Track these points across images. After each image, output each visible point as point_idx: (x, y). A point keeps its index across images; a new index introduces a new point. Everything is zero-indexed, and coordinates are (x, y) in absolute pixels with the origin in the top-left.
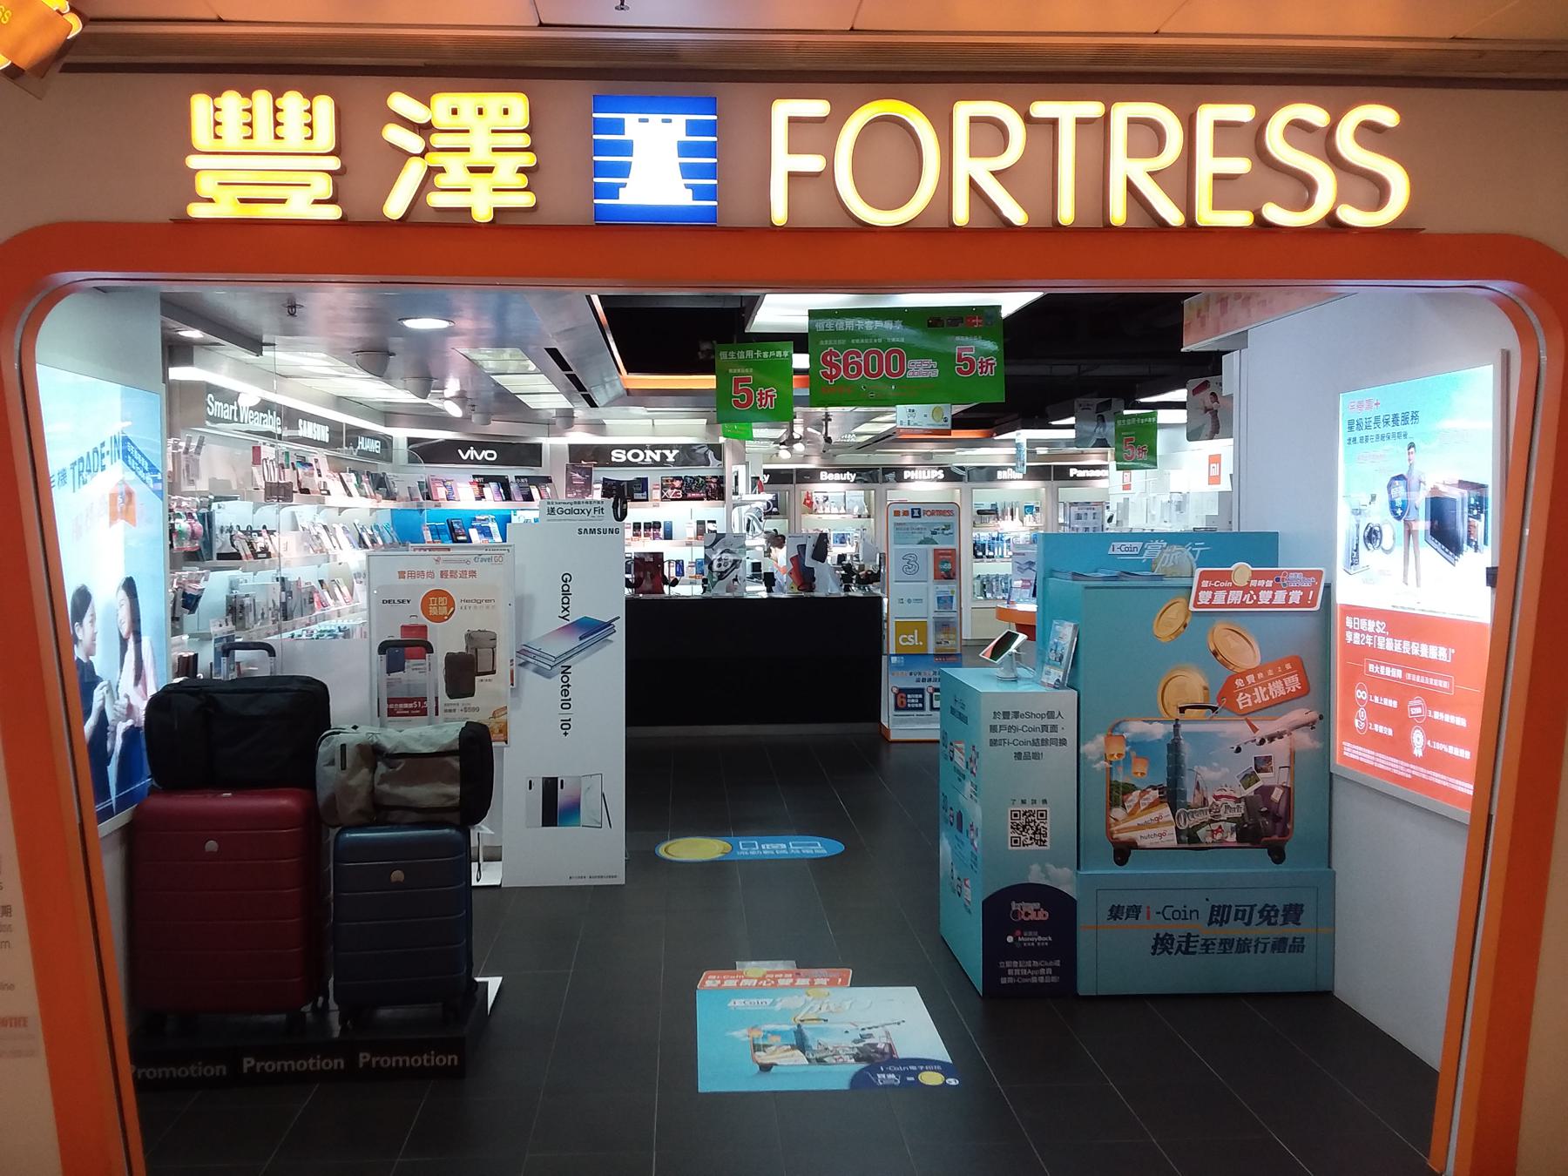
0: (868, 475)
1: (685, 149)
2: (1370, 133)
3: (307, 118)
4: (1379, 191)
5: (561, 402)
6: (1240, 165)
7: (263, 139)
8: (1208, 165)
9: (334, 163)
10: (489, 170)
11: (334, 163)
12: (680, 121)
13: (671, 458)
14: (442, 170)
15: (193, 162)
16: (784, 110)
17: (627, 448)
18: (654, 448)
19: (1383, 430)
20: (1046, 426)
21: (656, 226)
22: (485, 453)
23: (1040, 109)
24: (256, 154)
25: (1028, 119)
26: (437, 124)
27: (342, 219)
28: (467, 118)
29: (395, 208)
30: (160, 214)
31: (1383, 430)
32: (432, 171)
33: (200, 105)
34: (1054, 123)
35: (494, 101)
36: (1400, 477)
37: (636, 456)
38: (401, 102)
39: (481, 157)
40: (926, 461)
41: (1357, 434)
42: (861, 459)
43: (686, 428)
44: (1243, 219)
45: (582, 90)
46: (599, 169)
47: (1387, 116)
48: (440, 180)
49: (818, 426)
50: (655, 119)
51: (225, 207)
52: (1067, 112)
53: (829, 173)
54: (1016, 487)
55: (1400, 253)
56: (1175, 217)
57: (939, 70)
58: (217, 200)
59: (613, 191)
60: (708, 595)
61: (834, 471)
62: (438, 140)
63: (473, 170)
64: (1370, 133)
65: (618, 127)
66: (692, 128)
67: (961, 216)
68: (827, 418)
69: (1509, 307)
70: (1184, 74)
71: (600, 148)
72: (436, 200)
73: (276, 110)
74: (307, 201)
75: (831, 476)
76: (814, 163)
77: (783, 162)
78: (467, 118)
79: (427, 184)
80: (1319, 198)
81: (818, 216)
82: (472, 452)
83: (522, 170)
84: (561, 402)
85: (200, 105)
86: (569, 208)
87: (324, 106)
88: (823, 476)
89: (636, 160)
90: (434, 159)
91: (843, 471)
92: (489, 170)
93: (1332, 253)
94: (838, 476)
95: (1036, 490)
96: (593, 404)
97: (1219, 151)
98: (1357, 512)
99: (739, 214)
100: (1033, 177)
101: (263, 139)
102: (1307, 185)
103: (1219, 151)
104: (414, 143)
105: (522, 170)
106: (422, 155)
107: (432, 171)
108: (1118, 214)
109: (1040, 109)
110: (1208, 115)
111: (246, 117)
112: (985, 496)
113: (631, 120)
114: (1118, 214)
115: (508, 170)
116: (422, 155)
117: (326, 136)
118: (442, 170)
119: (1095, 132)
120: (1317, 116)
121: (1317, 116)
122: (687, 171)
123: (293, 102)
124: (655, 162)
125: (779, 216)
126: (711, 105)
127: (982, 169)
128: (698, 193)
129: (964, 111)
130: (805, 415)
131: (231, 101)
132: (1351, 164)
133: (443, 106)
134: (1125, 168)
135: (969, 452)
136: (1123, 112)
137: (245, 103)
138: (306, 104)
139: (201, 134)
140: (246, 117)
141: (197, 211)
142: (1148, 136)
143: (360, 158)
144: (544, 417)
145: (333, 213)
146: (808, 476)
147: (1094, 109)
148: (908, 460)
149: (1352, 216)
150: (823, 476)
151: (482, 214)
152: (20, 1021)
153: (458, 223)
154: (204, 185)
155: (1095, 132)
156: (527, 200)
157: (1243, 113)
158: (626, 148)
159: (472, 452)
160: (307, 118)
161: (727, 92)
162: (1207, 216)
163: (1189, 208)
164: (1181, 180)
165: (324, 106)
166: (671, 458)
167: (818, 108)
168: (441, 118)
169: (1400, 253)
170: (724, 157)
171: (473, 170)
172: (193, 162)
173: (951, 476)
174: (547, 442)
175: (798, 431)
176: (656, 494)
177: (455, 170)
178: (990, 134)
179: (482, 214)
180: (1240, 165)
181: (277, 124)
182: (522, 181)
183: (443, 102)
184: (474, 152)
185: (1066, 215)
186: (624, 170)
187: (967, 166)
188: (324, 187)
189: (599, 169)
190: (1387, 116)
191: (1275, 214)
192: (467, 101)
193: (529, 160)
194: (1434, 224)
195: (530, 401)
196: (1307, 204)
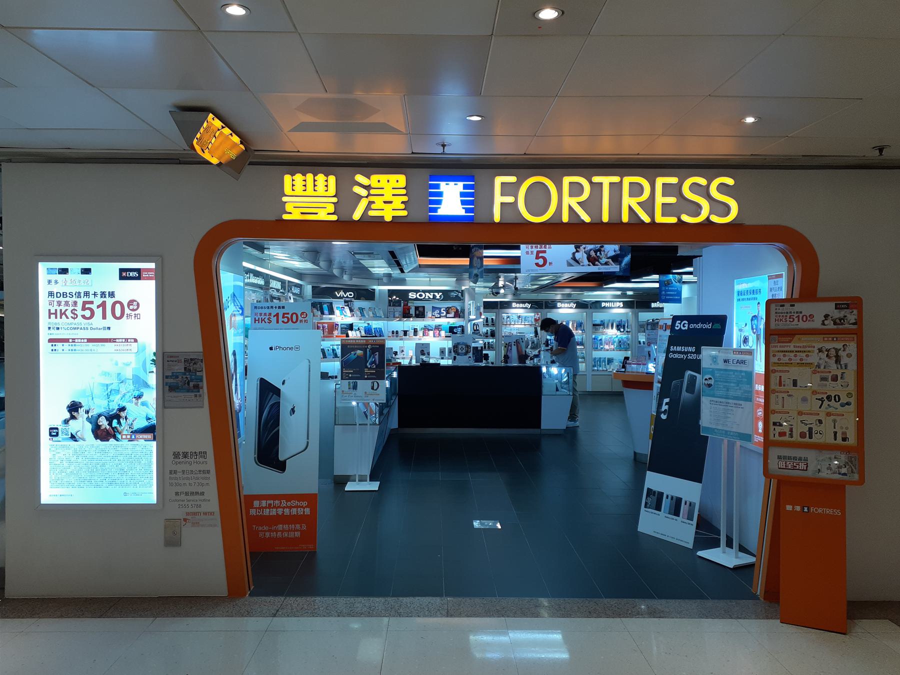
0: (537, 305)
1: (462, 195)
2: (722, 188)
3: (325, 183)
4: (727, 209)
5: (387, 270)
6: (672, 200)
7: (310, 190)
8: (660, 200)
9: (335, 200)
10: (391, 202)
11: (335, 200)
12: (461, 184)
13: (438, 297)
14: (374, 202)
15: (284, 199)
16: (499, 180)
17: (417, 291)
18: (429, 291)
19: (746, 297)
20: (629, 281)
21: (451, 222)
22: (348, 294)
23: (596, 179)
24: (308, 196)
25: (591, 182)
26: (373, 186)
27: (242, 157)
28: (383, 183)
29: (357, 216)
30: (272, 217)
31: (746, 297)
32: (371, 203)
33: (287, 178)
34: (601, 184)
35: (393, 178)
36: (755, 316)
37: (421, 295)
38: (360, 178)
39: (388, 197)
40: (567, 298)
41: (741, 297)
42: (534, 296)
43: (446, 283)
44: (673, 220)
45: (426, 173)
46: (432, 202)
47: (730, 181)
48: (373, 206)
49: (511, 281)
50: (452, 184)
51: (296, 216)
52: (606, 181)
53: (515, 203)
54: (618, 311)
55: (735, 233)
56: (646, 219)
57: (557, 166)
58: (293, 214)
59: (435, 210)
60: (456, 364)
61: (519, 303)
62: (372, 192)
63: (385, 202)
64: (722, 188)
65: (438, 186)
66: (465, 187)
67: (565, 218)
68: (516, 278)
69: (783, 252)
70: (651, 167)
71: (432, 194)
72: (371, 213)
73: (315, 181)
74: (326, 213)
75: (518, 305)
76: (511, 199)
77: (499, 199)
78: (383, 183)
79: (368, 208)
80: (703, 212)
81: (511, 219)
82: (342, 293)
83: (402, 202)
84: (387, 270)
85: (287, 178)
86: (420, 216)
87: (332, 179)
88: (514, 305)
89: (444, 199)
90: (371, 198)
91: (524, 303)
92: (391, 202)
93: (709, 232)
94: (521, 305)
95: (627, 313)
96: (402, 271)
97: (664, 195)
98: (741, 330)
99: (481, 218)
100: (591, 205)
101: (310, 190)
102: (699, 207)
103: (664, 195)
104: (364, 192)
105: (402, 202)
106: (367, 197)
107: (371, 203)
108: (625, 218)
109: (596, 179)
110: (660, 181)
111: (304, 183)
112: (598, 317)
113: (443, 184)
114: (625, 218)
115: (398, 202)
116: (367, 197)
117: (332, 190)
118: (374, 202)
119: (616, 189)
120: (703, 181)
121: (703, 181)
122: (463, 203)
123: (321, 178)
124: (451, 200)
125: (497, 218)
126: (472, 178)
127: (574, 202)
128: (467, 210)
129: (567, 180)
130: (505, 277)
131: (299, 177)
132: (714, 200)
133: (375, 180)
134: (628, 201)
135: (586, 293)
136: (627, 180)
137: (304, 178)
138: (325, 178)
139: (287, 189)
140: (304, 183)
141: (285, 217)
142: (636, 190)
143: (345, 198)
144: (376, 276)
145: (334, 218)
146: (506, 305)
147: (616, 179)
148: (559, 297)
149: (715, 219)
150: (514, 305)
151: (388, 218)
152: (212, 514)
153: (380, 221)
154: (289, 208)
155: (616, 189)
156: (405, 213)
157: (674, 180)
158: (440, 194)
159: (342, 293)
160: (325, 183)
161: (476, 172)
162: (659, 219)
163: (652, 216)
164: (649, 206)
165: (332, 179)
166: (438, 297)
167: (513, 179)
168: (374, 184)
169: (735, 233)
170: (476, 198)
171: (385, 202)
172: (284, 199)
173: (581, 305)
174: (377, 288)
175: (501, 283)
176: (429, 314)
177: (379, 202)
178: (576, 189)
179: (388, 218)
180: (672, 200)
181: (315, 186)
182: (403, 206)
183: (375, 178)
184: (386, 196)
185: (605, 218)
186: (439, 202)
187: (568, 201)
188: (331, 209)
189: (432, 202)
190: (730, 181)
191: (685, 218)
192: (383, 178)
193: (405, 199)
194: (748, 222)
195: (373, 270)
196: (698, 214)
